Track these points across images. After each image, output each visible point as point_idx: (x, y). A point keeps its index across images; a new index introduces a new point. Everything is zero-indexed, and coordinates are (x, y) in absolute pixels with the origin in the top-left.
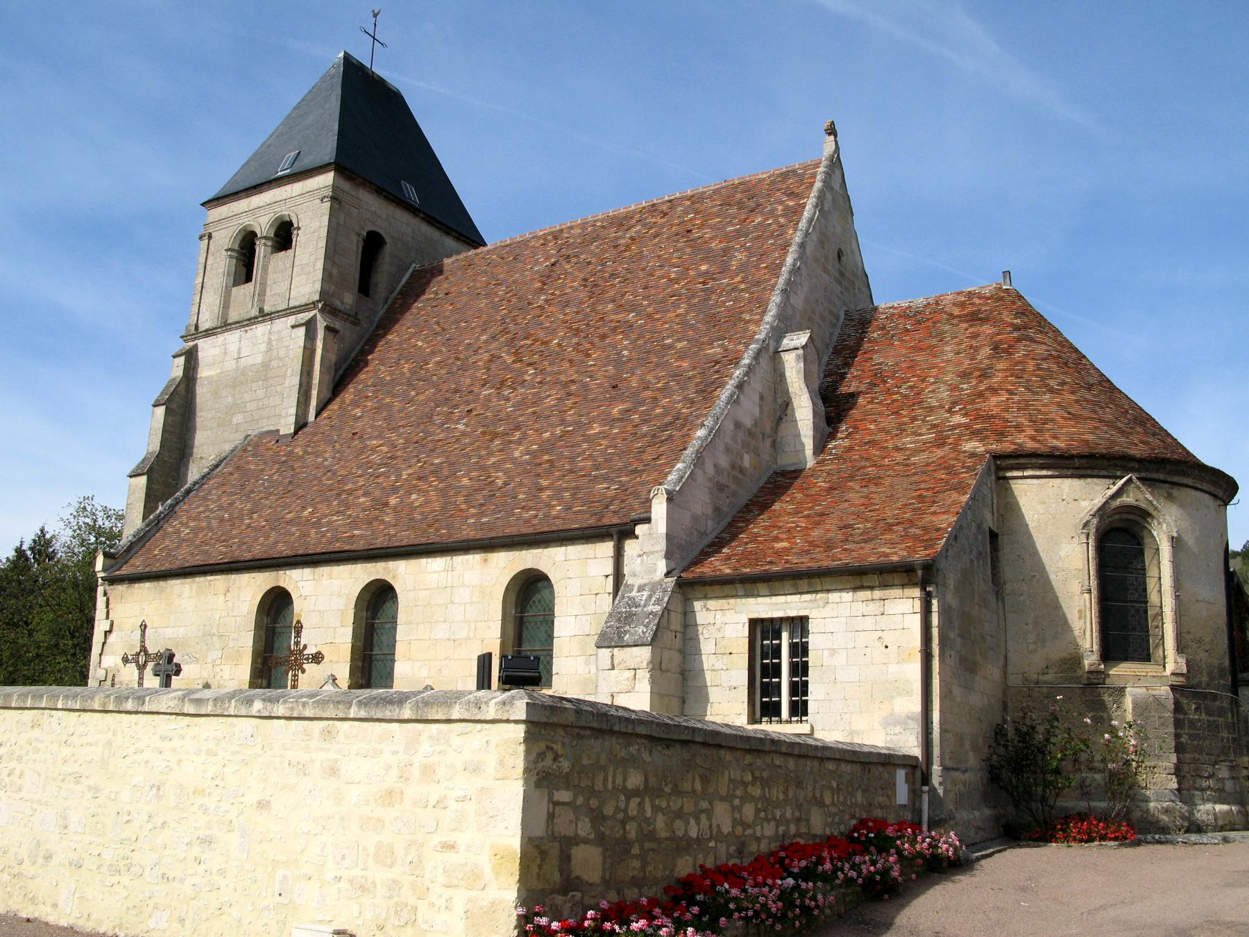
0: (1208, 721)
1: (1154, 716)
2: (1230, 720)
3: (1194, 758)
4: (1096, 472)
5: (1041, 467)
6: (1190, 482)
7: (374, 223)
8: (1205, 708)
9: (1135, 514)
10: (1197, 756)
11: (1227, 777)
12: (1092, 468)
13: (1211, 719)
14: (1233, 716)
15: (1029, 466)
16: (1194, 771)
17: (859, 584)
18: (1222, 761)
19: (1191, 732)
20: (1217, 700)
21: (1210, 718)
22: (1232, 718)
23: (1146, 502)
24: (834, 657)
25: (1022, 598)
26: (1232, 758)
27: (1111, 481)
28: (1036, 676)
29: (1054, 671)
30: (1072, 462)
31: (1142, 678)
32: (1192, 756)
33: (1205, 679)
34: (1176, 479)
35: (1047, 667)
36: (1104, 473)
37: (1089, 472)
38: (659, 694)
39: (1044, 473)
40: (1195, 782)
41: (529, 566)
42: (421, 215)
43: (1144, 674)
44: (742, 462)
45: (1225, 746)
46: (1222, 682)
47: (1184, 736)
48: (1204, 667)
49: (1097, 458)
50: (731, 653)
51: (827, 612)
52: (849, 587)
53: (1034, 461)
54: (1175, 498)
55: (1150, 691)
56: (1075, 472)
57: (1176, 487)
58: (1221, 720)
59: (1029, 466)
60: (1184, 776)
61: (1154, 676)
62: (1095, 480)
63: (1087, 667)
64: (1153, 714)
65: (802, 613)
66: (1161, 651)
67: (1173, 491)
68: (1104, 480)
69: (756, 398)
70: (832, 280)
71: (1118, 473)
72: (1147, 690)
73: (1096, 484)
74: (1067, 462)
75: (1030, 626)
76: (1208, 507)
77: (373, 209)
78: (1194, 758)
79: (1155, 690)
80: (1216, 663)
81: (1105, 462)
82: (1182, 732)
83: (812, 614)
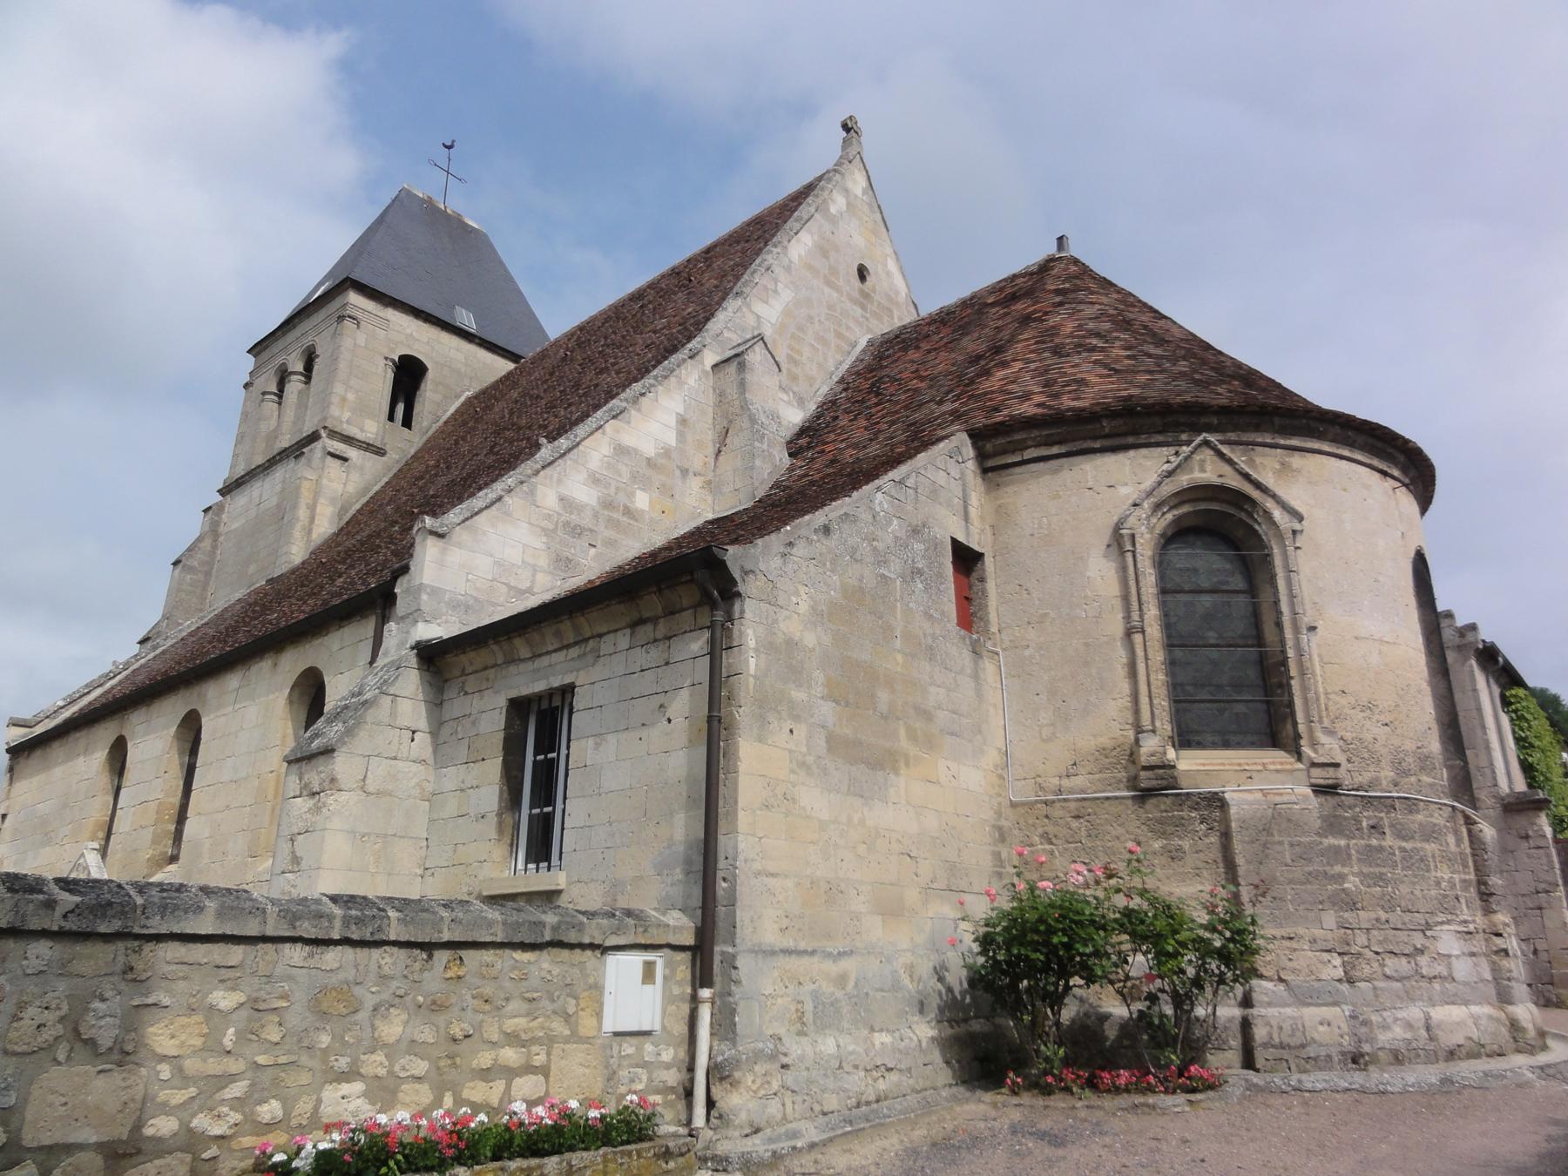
0: (1403, 850)
1: (1281, 843)
2: (1453, 847)
3: (1378, 920)
4: (1143, 439)
5: (1049, 443)
6: (1326, 447)
7: (409, 346)
8: (1392, 826)
9: (1223, 501)
10: (1383, 916)
11: (1456, 952)
12: (1135, 433)
13: (1408, 845)
14: (1459, 841)
15: (1030, 443)
16: (1380, 943)
17: (635, 616)
18: (1442, 923)
19: (1366, 870)
20: (1418, 812)
21: (1404, 844)
22: (1458, 845)
23: (1238, 477)
24: (601, 749)
25: (1027, 653)
26: (1462, 918)
27: (1172, 450)
28: (1056, 781)
29: (1088, 769)
30: (1098, 426)
31: (1254, 775)
32: (1373, 915)
33: (1387, 774)
34: (1295, 442)
35: (1075, 764)
36: (1160, 438)
37: (1130, 440)
38: (352, 832)
39: (1055, 450)
40: (1383, 965)
41: (319, 667)
42: (477, 341)
43: (1260, 768)
44: (633, 502)
45: (1446, 896)
46: (1426, 779)
47: (1351, 878)
48: (1384, 751)
49: (1139, 414)
50: (483, 760)
51: (597, 672)
52: (624, 624)
53: (1035, 433)
54: (1298, 471)
55: (1269, 797)
56: (1107, 442)
57: (1297, 454)
58: (1430, 848)
59: (1030, 443)
60: (1359, 954)
61: (1278, 771)
62: (1144, 451)
63: (1143, 759)
64: (1277, 838)
65: (567, 680)
66: (1289, 727)
67: (1292, 460)
68: (1159, 449)
69: (673, 421)
70: (843, 299)
71: (1184, 437)
72: (1265, 795)
73: (1145, 457)
74: (1090, 427)
75: (1044, 697)
76: (1368, 487)
77: (409, 331)
78: (1378, 920)
79: (1281, 794)
80: (1410, 746)
81: (1158, 421)
82: (1346, 870)
83: (580, 678)
